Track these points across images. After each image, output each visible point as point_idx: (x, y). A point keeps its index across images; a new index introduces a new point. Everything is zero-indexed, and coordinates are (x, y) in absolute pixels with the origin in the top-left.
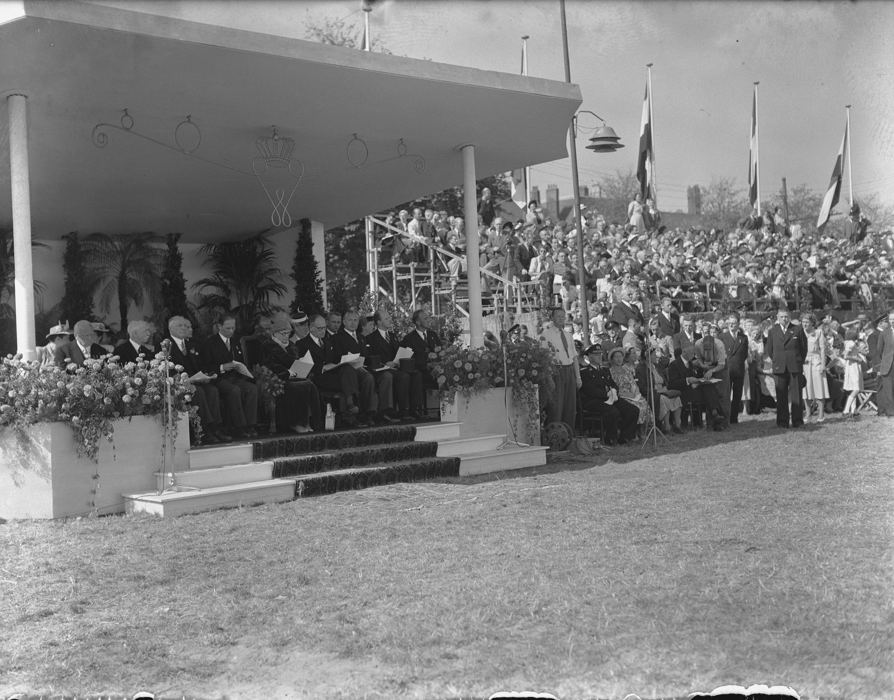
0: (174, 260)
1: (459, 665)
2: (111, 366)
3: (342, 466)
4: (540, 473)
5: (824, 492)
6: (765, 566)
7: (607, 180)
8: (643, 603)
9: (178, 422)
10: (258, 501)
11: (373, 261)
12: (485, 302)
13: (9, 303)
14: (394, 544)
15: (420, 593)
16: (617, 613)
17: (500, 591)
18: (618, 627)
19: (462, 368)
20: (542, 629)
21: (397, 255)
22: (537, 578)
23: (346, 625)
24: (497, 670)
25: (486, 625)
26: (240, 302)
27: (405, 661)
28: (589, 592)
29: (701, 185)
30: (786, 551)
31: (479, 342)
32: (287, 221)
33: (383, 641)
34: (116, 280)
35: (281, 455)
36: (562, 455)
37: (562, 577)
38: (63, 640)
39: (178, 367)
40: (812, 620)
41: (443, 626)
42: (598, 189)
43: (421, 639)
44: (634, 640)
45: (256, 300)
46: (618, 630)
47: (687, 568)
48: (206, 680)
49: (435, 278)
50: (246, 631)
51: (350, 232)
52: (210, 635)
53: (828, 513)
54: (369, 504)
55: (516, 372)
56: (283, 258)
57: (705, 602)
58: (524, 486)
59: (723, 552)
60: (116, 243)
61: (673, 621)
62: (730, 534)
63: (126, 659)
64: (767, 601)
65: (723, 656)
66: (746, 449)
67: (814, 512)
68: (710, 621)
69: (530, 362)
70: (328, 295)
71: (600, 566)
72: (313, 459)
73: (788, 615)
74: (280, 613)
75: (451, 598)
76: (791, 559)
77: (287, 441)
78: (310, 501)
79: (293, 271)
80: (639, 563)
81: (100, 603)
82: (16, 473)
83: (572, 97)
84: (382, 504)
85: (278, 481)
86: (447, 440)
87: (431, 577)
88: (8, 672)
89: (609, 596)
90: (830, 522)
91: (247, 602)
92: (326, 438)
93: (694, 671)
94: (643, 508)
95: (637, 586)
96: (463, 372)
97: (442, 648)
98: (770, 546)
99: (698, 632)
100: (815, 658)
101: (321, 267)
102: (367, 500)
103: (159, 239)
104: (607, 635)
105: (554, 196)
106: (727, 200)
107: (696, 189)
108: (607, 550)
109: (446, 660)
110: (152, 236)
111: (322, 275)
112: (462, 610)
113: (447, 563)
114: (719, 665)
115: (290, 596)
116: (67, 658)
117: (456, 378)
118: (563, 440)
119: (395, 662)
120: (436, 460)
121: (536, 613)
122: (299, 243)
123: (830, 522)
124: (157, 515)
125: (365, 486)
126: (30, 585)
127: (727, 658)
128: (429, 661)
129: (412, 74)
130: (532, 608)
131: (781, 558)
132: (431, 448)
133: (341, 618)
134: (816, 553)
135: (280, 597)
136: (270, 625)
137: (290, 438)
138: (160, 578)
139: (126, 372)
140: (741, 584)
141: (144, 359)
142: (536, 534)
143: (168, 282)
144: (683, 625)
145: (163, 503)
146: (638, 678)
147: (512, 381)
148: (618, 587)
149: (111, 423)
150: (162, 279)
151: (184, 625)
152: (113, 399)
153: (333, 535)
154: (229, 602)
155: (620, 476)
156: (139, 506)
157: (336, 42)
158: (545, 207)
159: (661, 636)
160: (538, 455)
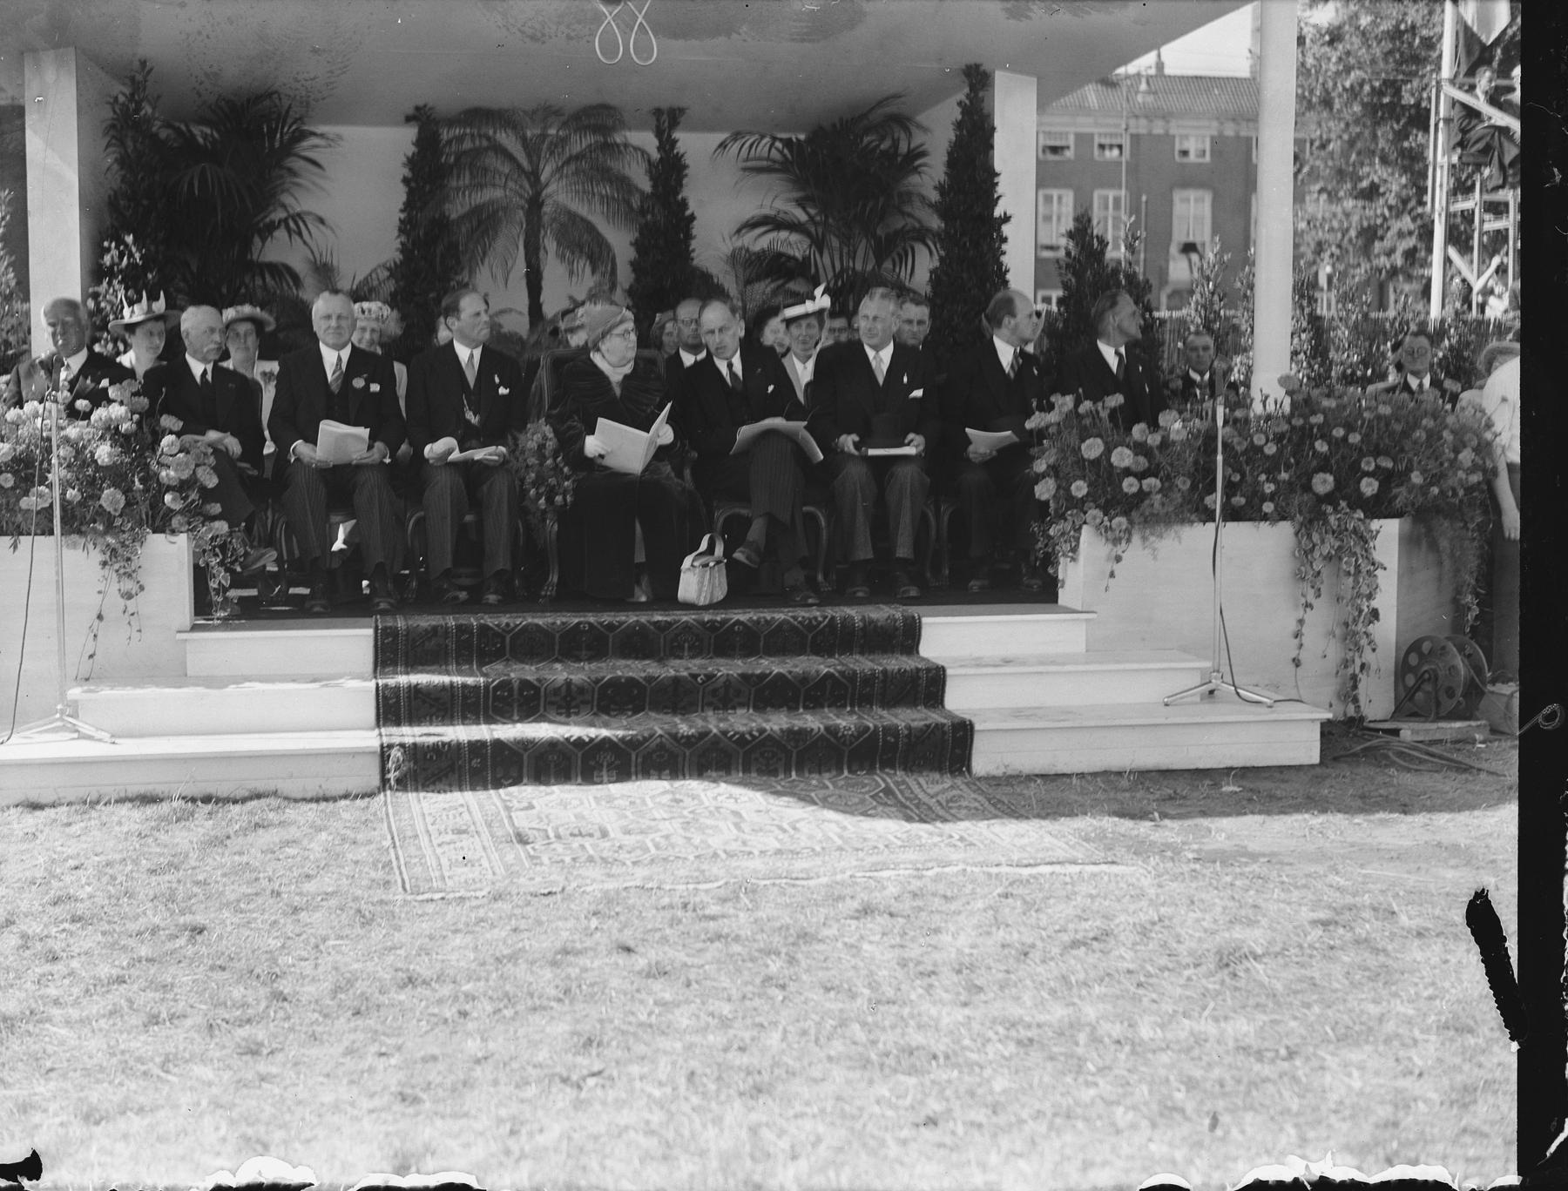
0: (670, 170)
31: (1278, 393)
77: (484, 629)
92: (611, 627)
117: (1080, 489)
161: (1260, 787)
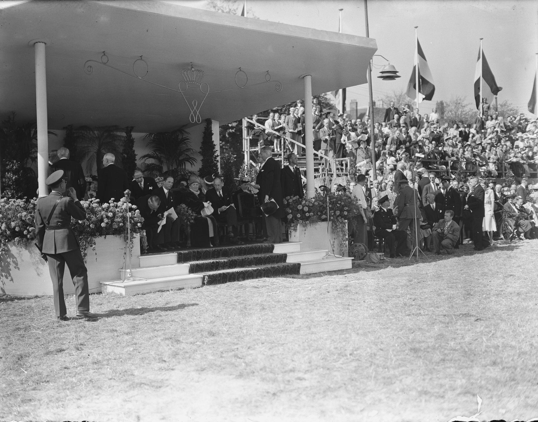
0: (130, 142)
1: (306, 384)
2: (95, 205)
3: (230, 267)
4: (348, 273)
5: (521, 287)
6: (487, 330)
7: (388, 97)
8: (415, 350)
9: (134, 240)
10: (181, 287)
11: (247, 144)
12: (316, 170)
13: (32, 167)
14: (263, 313)
15: (281, 342)
16: (399, 355)
17: (328, 342)
18: (400, 364)
19: (302, 210)
20: (354, 364)
21: (261, 141)
22: (350, 335)
23: (238, 360)
24: (329, 387)
25: (322, 361)
26: (168, 168)
27: (275, 380)
28: (382, 343)
29: (444, 101)
30: (499, 321)
32: (199, 120)
33: (261, 369)
34: (95, 154)
35: (194, 260)
36: (361, 262)
37: (365, 334)
38: (72, 366)
39: (134, 207)
40: (516, 361)
41: (295, 361)
42: (381, 103)
43: (283, 368)
44: (410, 371)
45: (178, 167)
46: (400, 366)
47: (440, 330)
48: (158, 390)
49: (284, 155)
50: (179, 363)
51: (232, 128)
52: (159, 364)
53: (524, 299)
54: (247, 289)
55: (335, 213)
56: (194, 142)
57: (451, 350)
58: (338, 280)
59: (461, 321)
60: (96, 132)
61: (433, 361)
62: (465, 310)
63: (110, 377)
64: (488, 350)
65: (464, 381)
66: (473, 261)
67: (515, 299)
68: (455, 361)
69: (343, 206)
70: (221, 164)
71: (387, 328)
72: (213, 262)
73: (502, 358)
74: (199, 352)
75: (299, 345)
76: (502, 326)
77: (198, 252)
78: (212, 288)
79: (201, 150)
80: (411, 327)
81: (91, 345)
82: (38, 268)
83: (371, 47)
84: (255, 290)
85: (193, 275)
86: (293, 253)
87: (287, 333)
88: (41, 384)
89: (394, 346)
90: (525, 304)
91: (179, 345)
92: (221, 250)
93: (446, 390)
94: (411, 295)
95: (410, 340)
96: (303, 212)
97: (296, 374)
98: (489, 318)
99: (447, 367)
100: (518, 383)
101: (217, 148)
102: (245, 287)
103: (122, 130)
104: (394, 368)
105: (354, 107)
106: (460, 110)
107: (442, 103)
108: (391, 319)
109: (298, 381)
110: (117, 128)
111: (218, 153)
112: (306, 352)
113: (296, 325)
114: (461, 386)
115: (203, 342)
116: (75, 376)
118: (362, 254)
119: (269, 382)
120: (286, 264)
121: (350, 355)
122: (204, 133)
123: (525, 304)
124: (121, 294)
125: (244, 279)
126: (49, 334)
127: (466, 382)
128: (289, 381)
129: (276, 32)
130: (348, 352)
131: (496, 325)
132: (283, 257)
133: (236, 356)
134: (517, 323)
135: (198, 343)
136: (193, 359)
137: (208, 249)
138: (126, 331)
139: (103, 209)
140: (472, 340)
141: (114, 201)
142: (348, 309)
143: (126, 156)
144: (439, 363)
145: (124, 287)
146: (414, 393)
147: (332, 218)
148: (399, 340)
149: (94, 239)
150: (122, 154)
151: (143, 358)
152: (96, 225)
153: (226, 308)
154: (168, 345)
155: (397, 276)
156: (110, 289)
157: (225, 11)
158: (349, 113)
159: (426, 369)
160: (347, 263)
161: (348, 271)
